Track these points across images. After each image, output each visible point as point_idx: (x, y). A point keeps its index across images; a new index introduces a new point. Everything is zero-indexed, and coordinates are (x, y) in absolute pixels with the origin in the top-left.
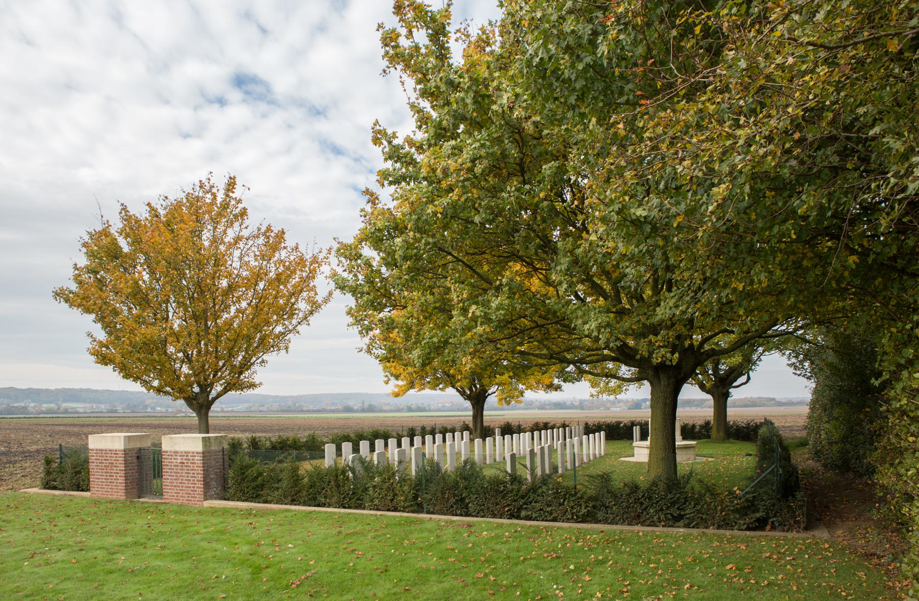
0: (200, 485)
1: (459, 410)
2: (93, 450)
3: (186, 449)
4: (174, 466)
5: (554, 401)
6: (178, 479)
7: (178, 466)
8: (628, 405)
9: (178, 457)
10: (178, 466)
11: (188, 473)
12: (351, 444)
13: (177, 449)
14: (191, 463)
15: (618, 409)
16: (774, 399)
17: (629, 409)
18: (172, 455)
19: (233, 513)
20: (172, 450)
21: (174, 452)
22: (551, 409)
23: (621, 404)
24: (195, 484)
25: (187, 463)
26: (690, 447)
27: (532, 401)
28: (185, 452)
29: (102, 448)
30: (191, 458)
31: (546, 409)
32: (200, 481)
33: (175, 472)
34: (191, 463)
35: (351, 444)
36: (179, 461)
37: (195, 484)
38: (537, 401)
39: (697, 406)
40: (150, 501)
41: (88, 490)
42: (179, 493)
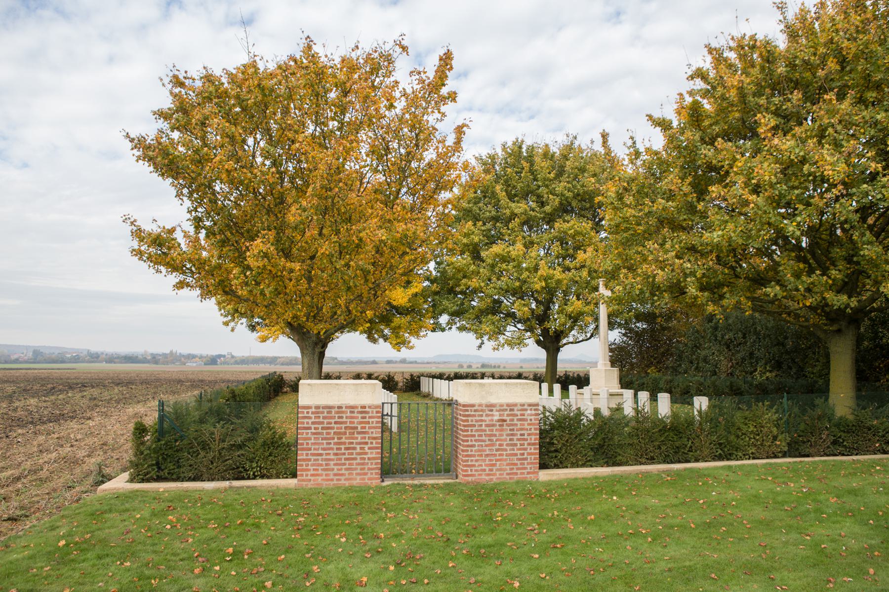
0: (535, 450)
1: (6, 362)
2: (309, 407)
3: (511, 401)
4: (487, 426)
5: (123, 354)
6: (493, 445)
7: (493, 425)
8: (204, 360)
9: (495, 413)
10: (493, 425)
11: (512, 435)
12: (639, 393)
13: (493, 400)
14: (519, 420)
15: (195, 364)
16: (336, 358)
17: (205, 364)
18: (482, 410)
19: (634, 485)
20: (484, 402)
21: (487, 406)
22: (121, 363)
23: (197, 359)
24: (525, 449)
25: (512, 420)
26: (617, 395)
27: (97, 353)
28: (508, 405)
29: (330, 403)
30: (519, 413)
31: (115, 363)
32: (534, 444)
33: (486, 435)
34: (519, 420)
35: (639, 393)
36: (496, 418)
37: (525, 449)
38: (102, 353)
39: (270, 363)
40: (406, 482)
41: (294, 475)
42: (494, 465)
